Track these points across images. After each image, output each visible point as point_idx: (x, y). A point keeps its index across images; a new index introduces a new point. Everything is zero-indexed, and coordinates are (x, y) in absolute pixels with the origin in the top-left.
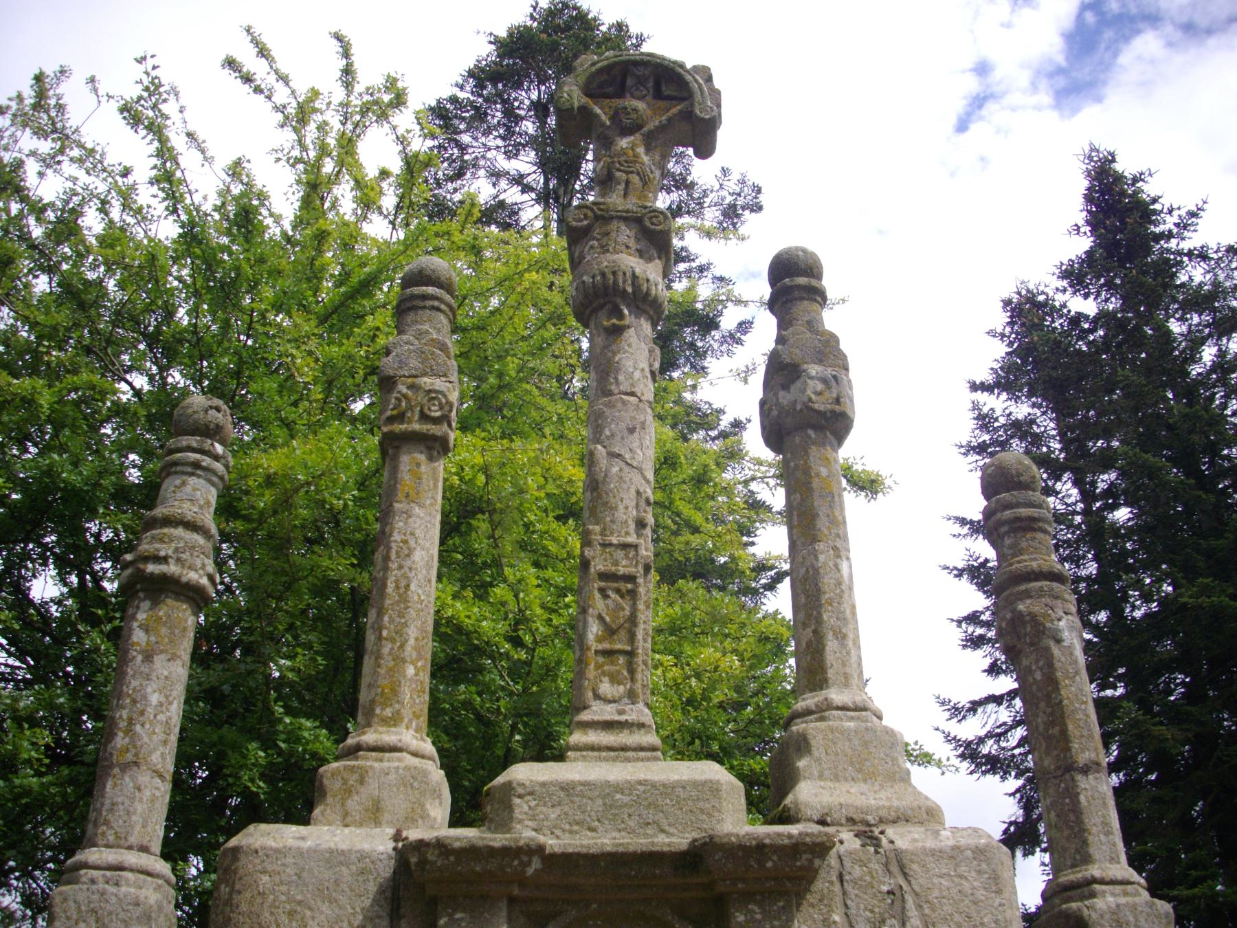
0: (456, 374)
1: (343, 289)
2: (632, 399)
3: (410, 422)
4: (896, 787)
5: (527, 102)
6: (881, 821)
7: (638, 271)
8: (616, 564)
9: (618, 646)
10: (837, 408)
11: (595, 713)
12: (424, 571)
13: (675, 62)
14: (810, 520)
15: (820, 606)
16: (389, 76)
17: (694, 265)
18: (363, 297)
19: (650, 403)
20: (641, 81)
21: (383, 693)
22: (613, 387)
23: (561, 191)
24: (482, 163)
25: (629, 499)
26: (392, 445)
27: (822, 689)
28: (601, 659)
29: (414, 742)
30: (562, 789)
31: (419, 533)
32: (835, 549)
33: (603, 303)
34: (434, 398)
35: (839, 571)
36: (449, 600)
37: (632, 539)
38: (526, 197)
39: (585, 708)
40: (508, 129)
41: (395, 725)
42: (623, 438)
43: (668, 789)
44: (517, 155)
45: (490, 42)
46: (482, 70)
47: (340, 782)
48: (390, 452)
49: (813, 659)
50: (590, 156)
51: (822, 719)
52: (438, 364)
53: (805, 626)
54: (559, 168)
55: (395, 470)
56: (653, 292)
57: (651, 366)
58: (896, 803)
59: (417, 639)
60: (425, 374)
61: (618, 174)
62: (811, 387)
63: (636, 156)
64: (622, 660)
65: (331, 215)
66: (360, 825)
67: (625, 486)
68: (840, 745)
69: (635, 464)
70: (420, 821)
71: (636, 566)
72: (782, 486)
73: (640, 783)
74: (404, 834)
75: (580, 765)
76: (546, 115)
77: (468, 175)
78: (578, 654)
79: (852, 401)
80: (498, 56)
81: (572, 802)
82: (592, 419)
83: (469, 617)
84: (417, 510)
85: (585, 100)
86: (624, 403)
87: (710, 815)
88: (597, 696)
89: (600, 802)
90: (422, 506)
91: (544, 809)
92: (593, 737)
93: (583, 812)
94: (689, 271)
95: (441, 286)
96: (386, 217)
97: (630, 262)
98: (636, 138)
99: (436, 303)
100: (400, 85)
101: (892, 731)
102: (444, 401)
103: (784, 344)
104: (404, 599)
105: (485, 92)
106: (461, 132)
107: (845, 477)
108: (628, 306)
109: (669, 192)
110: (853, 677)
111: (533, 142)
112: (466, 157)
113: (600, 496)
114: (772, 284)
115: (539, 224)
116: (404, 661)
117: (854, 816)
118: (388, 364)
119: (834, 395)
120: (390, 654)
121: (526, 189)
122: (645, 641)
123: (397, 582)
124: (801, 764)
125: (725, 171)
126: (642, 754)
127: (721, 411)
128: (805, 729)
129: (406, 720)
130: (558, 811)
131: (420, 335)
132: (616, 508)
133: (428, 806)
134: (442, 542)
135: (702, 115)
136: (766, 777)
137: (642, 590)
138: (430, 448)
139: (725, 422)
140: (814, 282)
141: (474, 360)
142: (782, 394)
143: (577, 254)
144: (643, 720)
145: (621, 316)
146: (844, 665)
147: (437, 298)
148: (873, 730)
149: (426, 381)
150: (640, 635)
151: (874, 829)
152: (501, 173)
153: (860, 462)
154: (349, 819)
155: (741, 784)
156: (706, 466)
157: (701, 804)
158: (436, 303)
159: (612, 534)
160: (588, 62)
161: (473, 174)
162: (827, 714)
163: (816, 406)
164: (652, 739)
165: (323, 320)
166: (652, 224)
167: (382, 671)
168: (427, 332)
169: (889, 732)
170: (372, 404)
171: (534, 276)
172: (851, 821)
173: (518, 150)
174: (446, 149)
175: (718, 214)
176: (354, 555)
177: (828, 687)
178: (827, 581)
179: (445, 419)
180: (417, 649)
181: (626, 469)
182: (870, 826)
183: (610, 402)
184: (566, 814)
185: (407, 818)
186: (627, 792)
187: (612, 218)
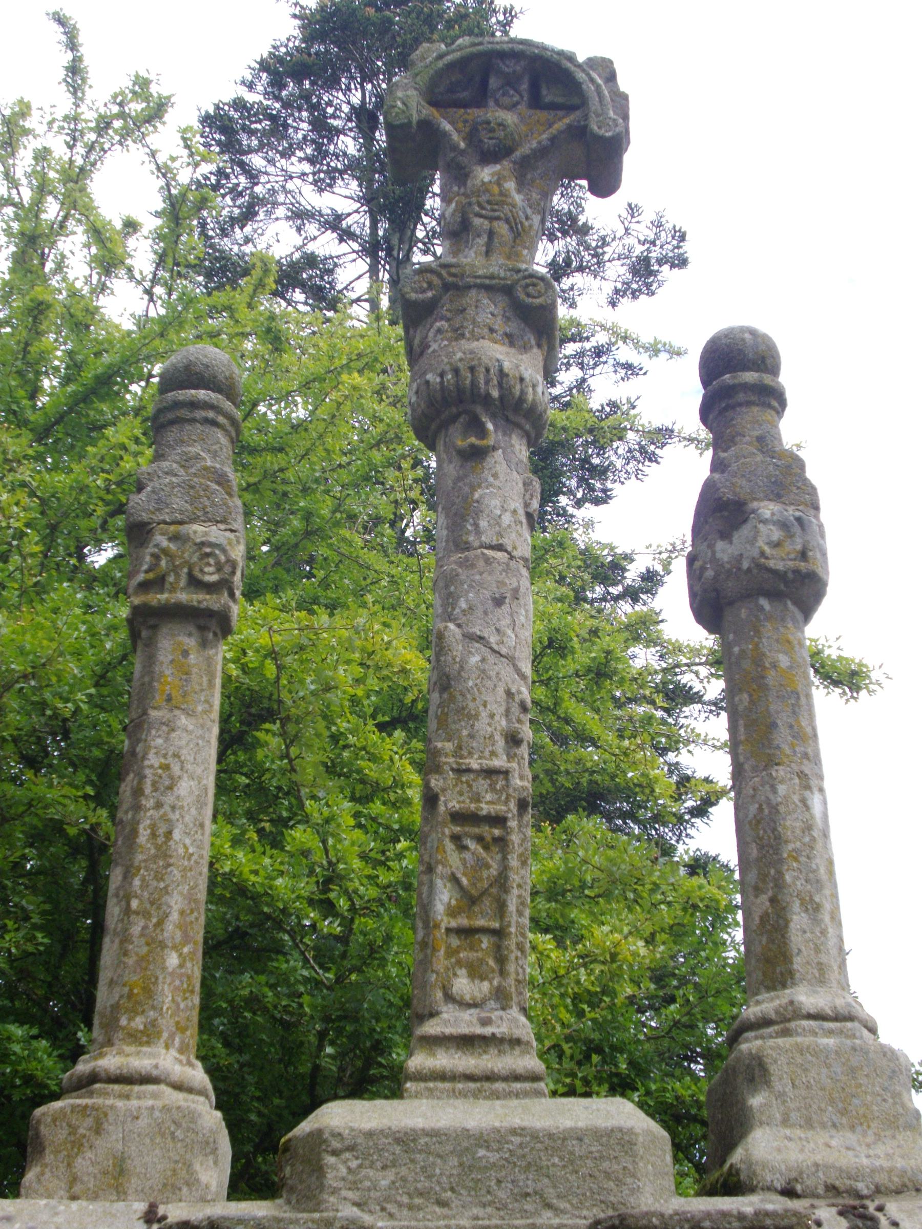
0: (240, 519)
1: (71, 388)
2: (499, 555)
3: (173, 590)
4: (900, 1137)
5: (346, 108)
6: (878, 1191)
7: (507, 365)
8: (477, 799)
9: (481, 922)
10: (802, 566)
11: (446, 1023)
12: (193, 811)
13: (561, 53)
14: (768, 739)
15: (781, 861)
16: (137, 76)
17: (587, 345)
18: (102, 400)
19: (526, 560)
20: (511, 82)
21: (130, 995)
22: (471, 538)
23: (395, 241)
24: (281, 198)
25: (496, 702)
26: (145, 623)
27: (784, 986)
28: (455, 942)
29: (178, 1068)
30: (398, 1141)
31: (185, 754)
32: (802, 775)
33: (456, 413)
34: (208, 555)
35: (807, 808)
36: (227, 848)
37: (499, 762)
38: (344, 248)
39: (433, 1014)
40: (319, 147)
41: (148, 1043)
42: (486, 613)
43: (555, 1141)
44: (330, 186)
45: (295, 16)
46: (280, 60)
47: (65, 1132)
48: (144, 634)
49: (771, 941)
50: (436, 188)
51: (786, 1033)
52: (213, 504)
53: (758, 891)
54: (394, 205)
55: (150, 660)
56: (530, 397)
57: (526, 505)
58: (900, 1163)
59: (182, 913)
60: (194, 520)
61: (477, 221)
62: (762, 537)
63: (504, 194)
64: (486, 942)
65: (54, 282)
66: (94, 1197)
67: (489, 684)
68: (813, 1073)
69: (504, 651)
70: (185, 1189)
71: (506, 802)
72: (718, 677)
73: (514, 1132)
74: (161, 1210)
75: (424, 1105)
76: (374, 128)
77: (261, 216)
78: (421, 934)
79: (824, 554)
80: (304, 40)
81: (412, 1161)
82: (441, 584)
83: (256, 872)
84: (183, 720)
85: (429, 111)
86: (488, 561)
87: (619, 1182)
88: (449, 997)
89: (454, 1161)
90: (190, 714)
91: (371, 1173)
92: (443, 1060)
93: (429, 1177)
94: (581, 354)
95: (217, 389)
96: (139, 283)
97: (496, 353)
98: (503, 167)
99: (211, 414)
100: (154, 89)
101: (893, 1051)
102: (223, 558)
103: (723, 472)
104: (163, 853)
105: (284, 93)
106: (250, 151)
107: (813, 666)
108: (493, 417)
109: (552, 238)
110: (830, 968)
111: (353, 167)
112: (258, 189)
113: (452, 698)
114: (705, 383)
115: (362, 287)
116: (163, 945)
117: (837, 1183)
118: (140, 504)
119: (799, 547)
120: (142, 935)
121: (346, 235)
122: (520, 914)
123: (153, 827)
124: (756, 1101)
125: (632, 209)
126: (518, 1086)
127: (628, 558)
128: (759, 1049)
129: (165, 1035)
130: (391, 1175)
131: (187, 461)
132: (476, 717)
133: (197, 1167)
134: (221, 758)
135: (602, 132)
136: (700, 1108)
137: (515, 838)
138: (202, 629)
139: (632, 574)
140: (767, 379)
141: (268, 492)
142: (720, 545)
143: (417, 342)
144: (517, 1033)
145: (482, 432)
146: (817, 950)
147: (212, 407)
148: (863, 1051)
149: (197, 530)
150: (512, 906)
151: (867, 1202)
152: (307, 213)
153: (836, 645)
154: (77, 1189)
155: (665, 1134)
156: (608, 653)
157: (606, 1165)
158: (211, 414)
159: (470, 754)
160: (432, 53)
161: (269, 213)
162: (792, 1025)
163: (771, 564)
164: (531, 1062)
165: (41, 434)
166: (528, 295)
167: (130, 961)
168: (197, 457)
169: (889, 1054)
170: (118, 557)
171: (357, 379)
172: (832, 1190)
173: (333, 179)
174: (227, 177)
175: (623, 270)
176: (89, 782)
177: (794, 984)
178: (791, 824)
179: (225, 585)
180: (183, 927)
181: (492, 658)
182: (862, 1197)
183: (467, 559)
184: (404, 1179)
185: (165, 1185)
186: (495, 1146)
187: (469, 287)
